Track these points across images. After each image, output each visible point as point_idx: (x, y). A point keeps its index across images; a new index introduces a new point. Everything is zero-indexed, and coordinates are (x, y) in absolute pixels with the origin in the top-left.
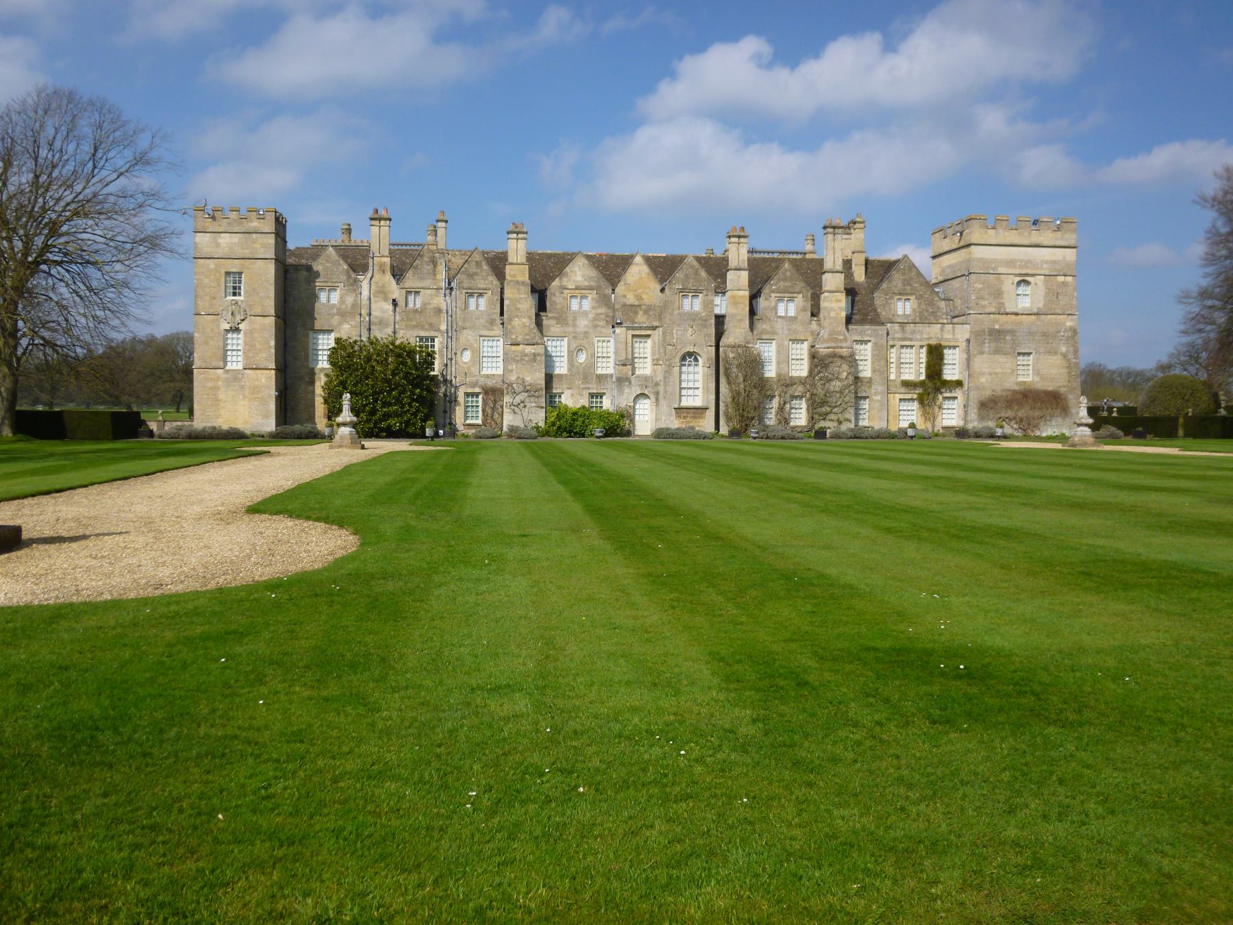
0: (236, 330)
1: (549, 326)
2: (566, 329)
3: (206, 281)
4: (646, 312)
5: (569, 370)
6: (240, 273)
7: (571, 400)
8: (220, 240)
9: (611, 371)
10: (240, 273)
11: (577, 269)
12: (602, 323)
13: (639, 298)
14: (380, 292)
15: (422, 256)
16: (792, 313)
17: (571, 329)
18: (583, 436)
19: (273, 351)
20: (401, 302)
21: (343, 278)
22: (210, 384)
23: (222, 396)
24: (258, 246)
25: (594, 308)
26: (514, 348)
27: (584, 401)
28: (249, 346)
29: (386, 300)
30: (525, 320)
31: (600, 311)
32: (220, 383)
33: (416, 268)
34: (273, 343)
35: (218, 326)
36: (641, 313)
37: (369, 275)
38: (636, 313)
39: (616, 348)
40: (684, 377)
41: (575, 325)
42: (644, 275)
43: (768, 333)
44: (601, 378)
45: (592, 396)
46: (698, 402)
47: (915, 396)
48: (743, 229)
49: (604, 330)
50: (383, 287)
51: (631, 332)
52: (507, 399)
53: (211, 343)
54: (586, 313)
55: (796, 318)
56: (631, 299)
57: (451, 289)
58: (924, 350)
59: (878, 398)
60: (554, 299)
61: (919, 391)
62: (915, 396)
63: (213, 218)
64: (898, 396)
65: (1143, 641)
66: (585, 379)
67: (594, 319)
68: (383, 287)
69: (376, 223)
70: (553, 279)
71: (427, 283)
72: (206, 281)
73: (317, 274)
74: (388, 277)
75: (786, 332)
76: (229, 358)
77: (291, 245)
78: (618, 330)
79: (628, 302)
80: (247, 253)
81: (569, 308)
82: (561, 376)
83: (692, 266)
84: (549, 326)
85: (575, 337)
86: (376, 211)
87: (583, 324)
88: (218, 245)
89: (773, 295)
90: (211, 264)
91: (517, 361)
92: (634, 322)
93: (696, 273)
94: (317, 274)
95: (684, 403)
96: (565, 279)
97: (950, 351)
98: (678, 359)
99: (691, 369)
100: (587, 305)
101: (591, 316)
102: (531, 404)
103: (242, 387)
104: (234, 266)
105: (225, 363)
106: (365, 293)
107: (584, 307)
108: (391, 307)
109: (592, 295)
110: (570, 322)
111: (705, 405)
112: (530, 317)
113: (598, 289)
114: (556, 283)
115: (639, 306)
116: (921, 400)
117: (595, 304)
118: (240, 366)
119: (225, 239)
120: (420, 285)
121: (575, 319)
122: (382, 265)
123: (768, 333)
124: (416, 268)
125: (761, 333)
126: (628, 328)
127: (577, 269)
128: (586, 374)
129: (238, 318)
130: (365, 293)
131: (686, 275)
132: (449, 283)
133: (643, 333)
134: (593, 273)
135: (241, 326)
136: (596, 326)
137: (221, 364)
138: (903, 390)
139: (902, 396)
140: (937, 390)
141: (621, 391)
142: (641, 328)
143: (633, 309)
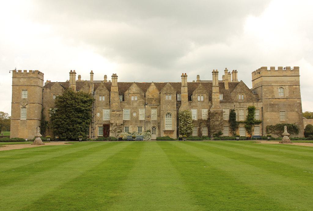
9: (143, 119)
12: (142, 104)
23: (19, 128)
25: (138, 99)
38: (152, 101)
41: (133, 105)
46: (170, 129)
48: (185, 74)
56: (150, 96)
60: (126, 97)
67: (139, 103)
80: (29, 84)
87: (135, 104)
88: (20, 82)
89: (196, 94)
110: (132, 104)
113: (140, 93)
135: (27, 107)
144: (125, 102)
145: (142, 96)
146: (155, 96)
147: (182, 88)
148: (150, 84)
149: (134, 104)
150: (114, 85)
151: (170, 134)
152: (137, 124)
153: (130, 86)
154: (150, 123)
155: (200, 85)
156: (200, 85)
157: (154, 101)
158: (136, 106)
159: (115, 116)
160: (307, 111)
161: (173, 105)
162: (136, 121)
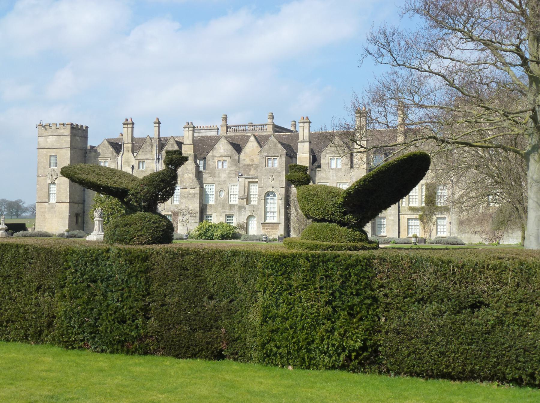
0: (53, 183)
1: (206, 178)
2: (215, 179)
3: (42, 160)
4: (255, 169)
5: (215, 202)
6: (56, 155)
7: (216, 219)
8: (48, 140)
9: (237, 203)
10: (56, 155)
11: (221, 146)
12: (233, 175)
13: (252, 160)
14: (127, 162)
15: (146, 142)
16: (339, 166)
17: (217, 179)
18: (212, 238)
19: (68, 193)
20: (136, 167)
21: (110, 155)
22: (42, 210)
23: (47, 216)
24: (63, 142)
25: (229, 167)
26: (184, 190)
27: (222, 220)
28: (59, 191)
29: (129, 166)
30: (191, 175)
31: (232, 169)
32: (46, 210)
33: (143, 149)
34: (68, 190)
35: (46, 182)
36: (253, 169)
37: (121, 153)
38: (250, 169)
39: (240, 189)
40: (268, 205)
41: (219, 177)
42: (255, 147)
43: (324, 178)
44: (231, 206)
45: (227, 216)
46: (275, 221)
47: (418, 217)
48: (308, 118)
49: (234, 179)
50: (128, 159)
51: (247, 180)
52: (180, 218)
53: (44, 190)
54: (225, 170)
55: (341, 169)
56: (248, 162)
57: (159, 159)
58: (424, 187)
59: (392, 218)
60: (209, 163)
61: (420, 213)
62: (418, 217)
63: (46, 129)
64: (407, 217)
65: (256, 389)
66: (223, 207)
67: (229, 173)
68: (128, 159)
69: (126, 126)
70: (208, 153)
71: (148, 156)
72: (42, 160)
73: (99, 154)
74: (130, 154)
75: (335, 178)
76: (51, 197)
77: (161, 136)
78: (240, 179)
79: (246, 163)
80: (58, 145)
81: (217, 167)
82: (211, 205)
83: (273, 142)
84: (206, 178)
85: (219, 184)
86: (127, 120)
87: (223, 176)
88: (47, 142)
89: (328, 156)
90: (44, 151)
91: (185, 197)
92: (249, 174)
93: (275, 145)
94: (99, 154)
95: (267, 221)
96: (215, 152)
97: (211, 196)
98: (263, 196)
99: (272, 201)
100: (226, 165)
101: (227, 172)
102: (192, 220)
103: (55, 212)
104: (53, 152)
105: (49, 200)
106: (120, 162)
107: (225, 166)
108: (131, 170)
109: (228, 160)
110: (217, 175)
111: (278, 222)
112: (193, 174)
113: (231, 157)
114: (210, 154)
115: (252, 165)
116: (421, 219)
117: (229, 165)
118: (55, 202)
119: (50, 139)
120: (145, 158)
121: (219, 173)
122: (128, 148)
123: (324, 178)
124: (143, 149)
125: (320, 179)
126: (246, 178)
127: (221, 146)
128: (226, 204)
129: (54, 177)
130: (120, 162)
131: (270, 147)
132: (159, 156)
133: (254, 180)
134: (230, 147)
135: (56, 182)
136: (230, 177)
137: (47, 200)
138: (410, 213)
139: (409, 217)
140: (432, 213)
141: (240, 213)
142: (252, 178)
143: (249, 166)
144: (207, 172)
145: (235, 160)
146: (255, 160)
147: (300, 145)
148: (145, 139)
149: (221, 175)
150: (187, 143)
151: (272, 229)
152: (226, 211)
153: (113, 143)
154: (245, 209)
155: (337, 138)
156: (337, 138)
157: (253, 169)
158: (224, 179)
159: (188, 197)
160: (4, 198)
161: (279, 176)
162: (223, 206)
